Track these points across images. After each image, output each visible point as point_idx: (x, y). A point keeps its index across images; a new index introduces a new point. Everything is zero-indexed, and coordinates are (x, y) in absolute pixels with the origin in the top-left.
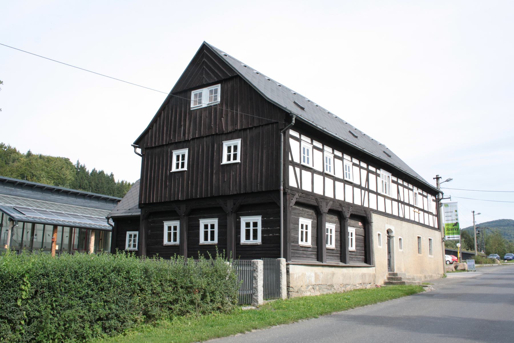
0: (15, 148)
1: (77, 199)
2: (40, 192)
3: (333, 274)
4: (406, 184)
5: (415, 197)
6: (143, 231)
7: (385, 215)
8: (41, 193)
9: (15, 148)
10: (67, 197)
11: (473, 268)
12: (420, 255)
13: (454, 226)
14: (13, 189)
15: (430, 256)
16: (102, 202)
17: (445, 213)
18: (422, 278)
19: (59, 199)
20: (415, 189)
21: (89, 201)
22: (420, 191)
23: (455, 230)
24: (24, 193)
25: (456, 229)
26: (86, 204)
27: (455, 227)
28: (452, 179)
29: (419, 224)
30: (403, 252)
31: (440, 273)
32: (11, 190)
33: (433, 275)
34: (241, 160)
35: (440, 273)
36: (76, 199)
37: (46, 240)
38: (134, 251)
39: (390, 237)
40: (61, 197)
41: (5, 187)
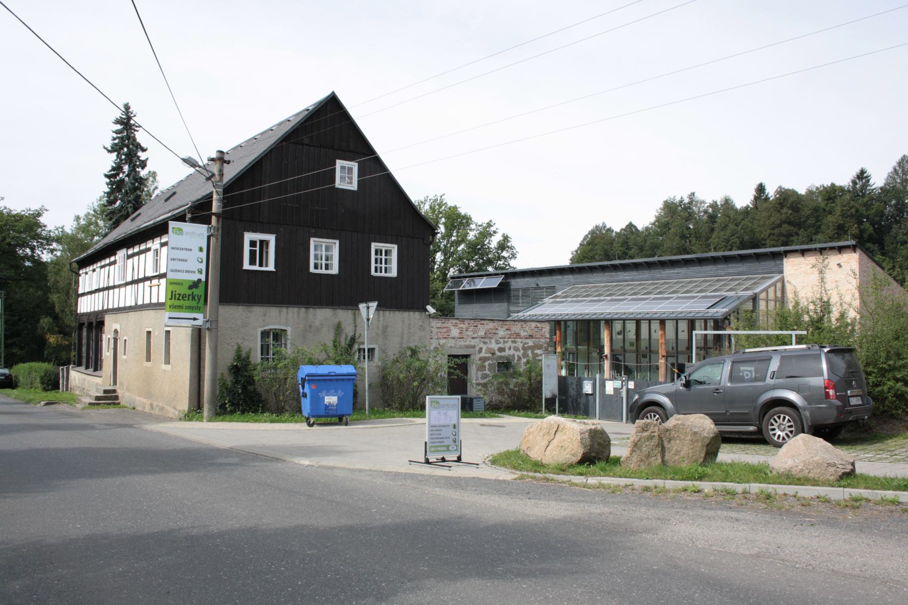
1: (704, 267)
4: (136, 249)
5: (157, 260)
7: (146, 307)
12: (149, 364)
13: (190, 287)
16: (749, 262)
17: (171, 262)
19: (673, 273)
20: (149, 244)
23: (193, 298)
25: (196, 298)
26: (731, 271)
27: (194, 290)
28: (126, 124)
33: (167, 407)
34: (276, 267)
36: (700, 268)
38: (603, 320)
39: (116, 340)
40: (676, 271)
41: (606, 274)
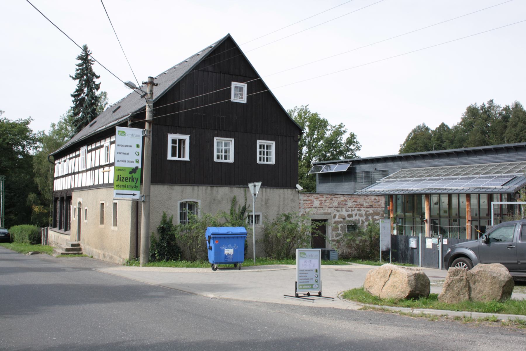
0: (423, 124)
1: (499, 155)
2: (456, 157)
3: (485, 266)
5: (108, 153)
6: (141, 210)
8: (457, 158)
9: (423, 124)
10: (486, 156)
11: (313, 282)
12: (102, 226)
14: (432, 160)
15: (113, 228)
18: (101, 255)
19: (476, 160)
20: (103, 143)
21: (514, 154)
22: (108, 140)
24: (441, 162)
25: (135, 180)
29: (99, 186)
30: (86, 223)
31: (123, 257)
32: (431, 162)
33: (115, 256)
35: (123, 257)
36: (496, 155)
37: (442, 206)
40: (478, 158)
41: (425, 161)
